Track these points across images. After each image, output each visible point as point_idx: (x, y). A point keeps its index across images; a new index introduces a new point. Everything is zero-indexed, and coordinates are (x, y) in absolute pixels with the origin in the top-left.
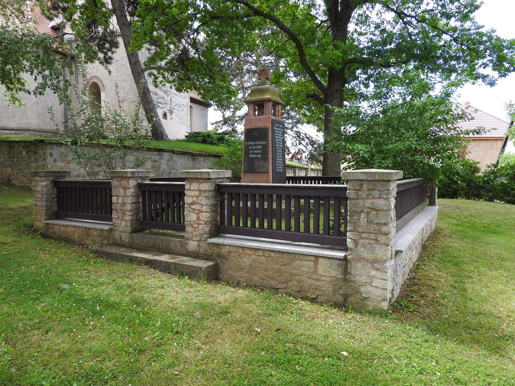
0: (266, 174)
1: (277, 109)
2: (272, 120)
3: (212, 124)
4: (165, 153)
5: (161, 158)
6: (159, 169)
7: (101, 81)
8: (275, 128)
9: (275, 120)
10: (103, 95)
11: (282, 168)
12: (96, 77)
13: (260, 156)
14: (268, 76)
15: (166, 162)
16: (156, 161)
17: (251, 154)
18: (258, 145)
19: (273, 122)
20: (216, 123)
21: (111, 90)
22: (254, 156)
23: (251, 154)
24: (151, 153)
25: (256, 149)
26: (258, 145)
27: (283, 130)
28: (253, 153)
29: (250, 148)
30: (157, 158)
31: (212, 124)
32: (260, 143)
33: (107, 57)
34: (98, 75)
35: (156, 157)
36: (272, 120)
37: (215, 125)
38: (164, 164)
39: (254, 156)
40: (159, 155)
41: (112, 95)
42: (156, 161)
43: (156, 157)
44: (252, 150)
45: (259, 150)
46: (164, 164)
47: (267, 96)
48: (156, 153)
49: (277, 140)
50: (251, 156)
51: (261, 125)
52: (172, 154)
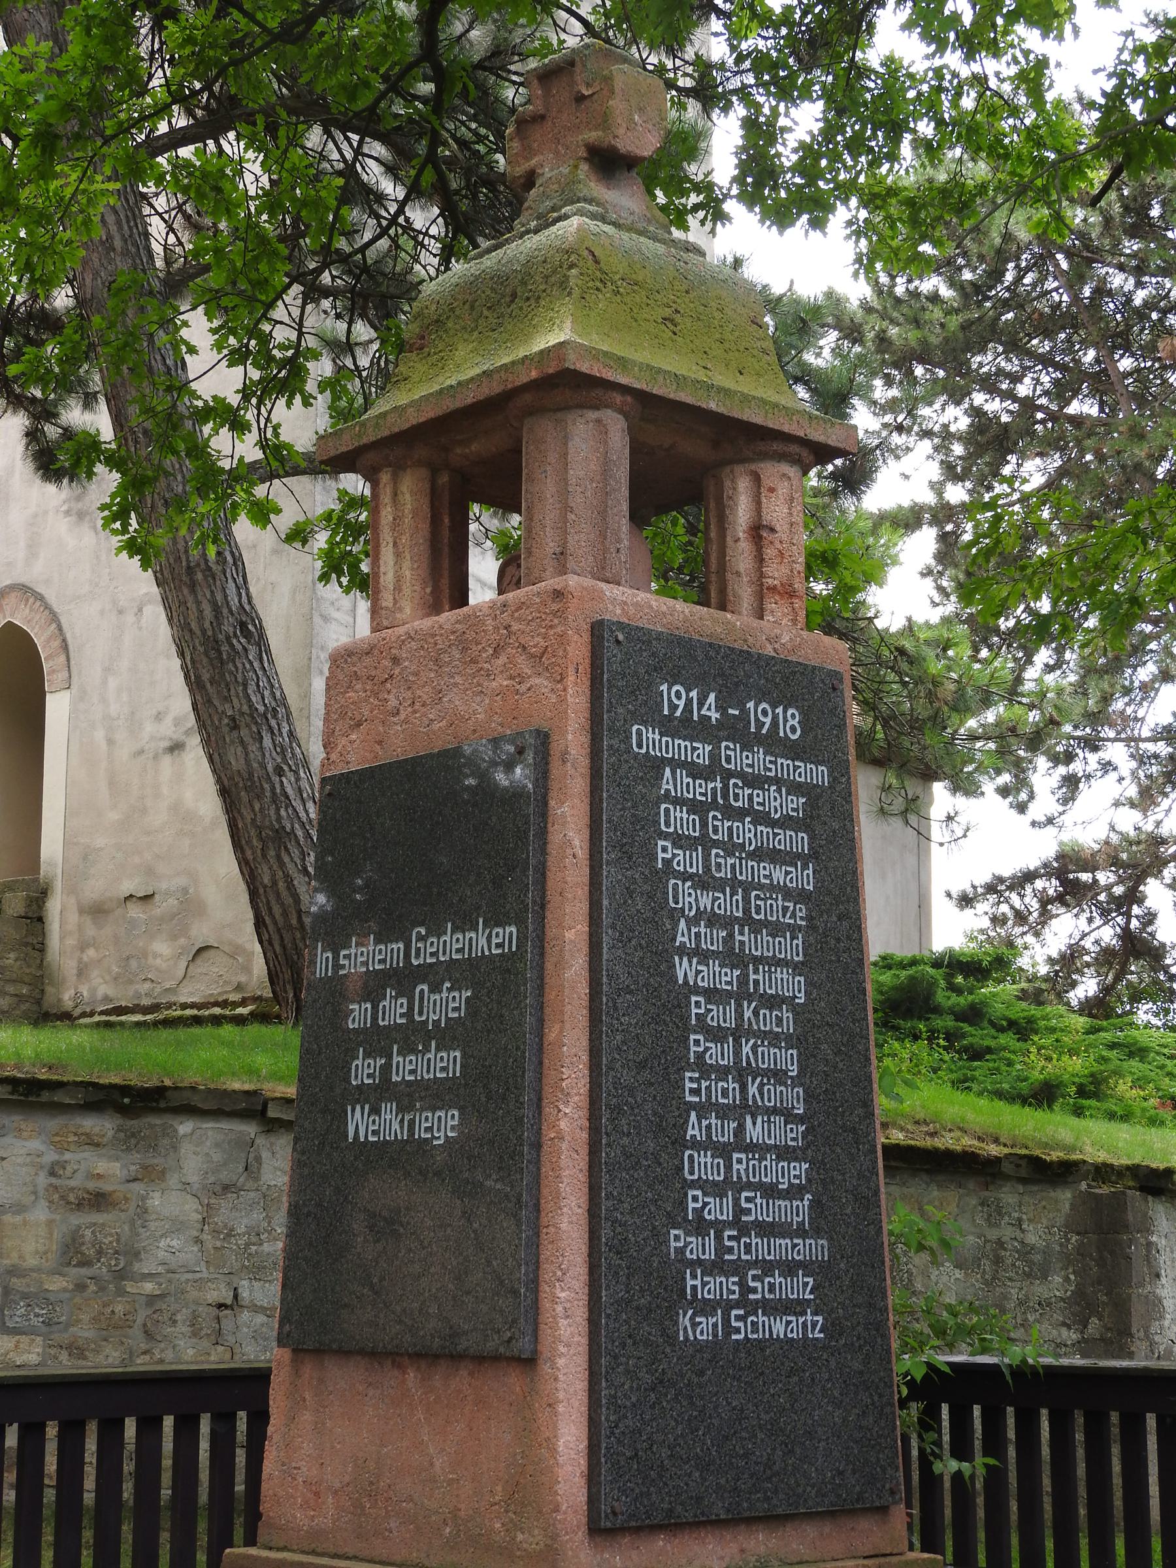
0: (514, 1380)
1: (742, 514)
2: (598, 630)
3: (966, 901)
4: (185, 1127)
5: (150, 1175)
6: (121, 1275)
7: (54, 618)
8: (649, 740)
9: (638, 637)
10: (58, 708)
11: (802, 1287)
12: (25, 591)
13: (442, 1126)
14: (604, 121)
15: (190, 1209)
16: (99, 1200)
17: (362, 1095)
18: (433, 975)
19: (623, 668)
20: (991, 888)
21: (108, 670)
22: (390, 1124)
23: (362, 1095)
24: (53, 1123)
25: (413, 1036)
26: (433, 975)
27: (817, 774)
28: (381, 1092)
29: (358, 1014)
30: (110, 1168)
31: (966, 901)
32: (452, 944)
33: (52, 432)
34: (34, 575)
35: (102, 1166)
36: (598, 630)
37: (983, 907)
38: (177, 1226)
39: (390, 1124)
40: (128, 1142)
41: (114, 709)
42: (99, 1200)
43: (102, 1166)
44: (378, 1040)
45: (446, 1036)
46: (177, 1226)
47: (556, 333)
48: (101, 1125)
49: (689, 898)
50: (359, 1124)
51: (461, 711)
52: (250, 1129)
